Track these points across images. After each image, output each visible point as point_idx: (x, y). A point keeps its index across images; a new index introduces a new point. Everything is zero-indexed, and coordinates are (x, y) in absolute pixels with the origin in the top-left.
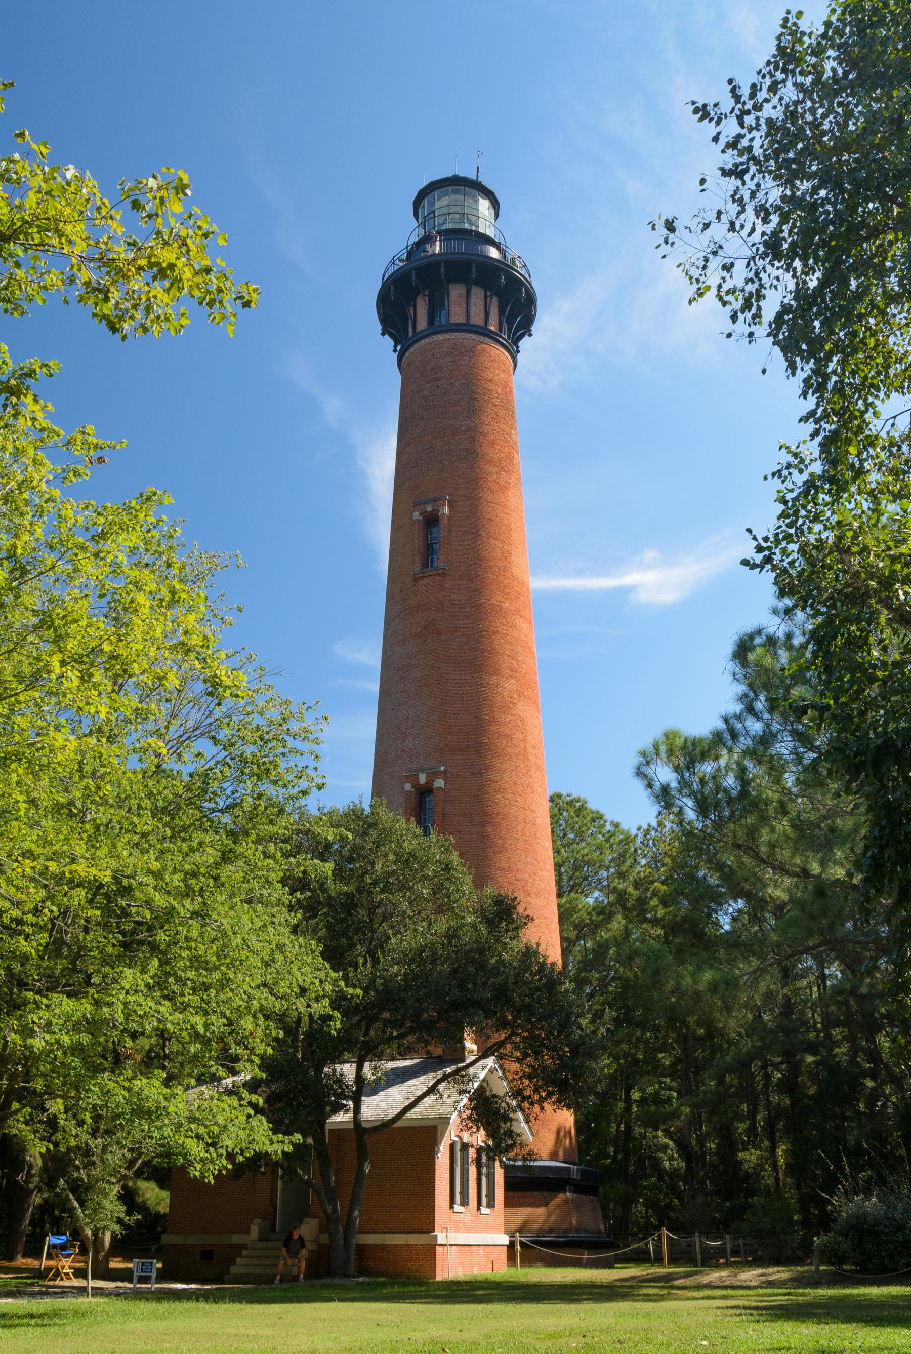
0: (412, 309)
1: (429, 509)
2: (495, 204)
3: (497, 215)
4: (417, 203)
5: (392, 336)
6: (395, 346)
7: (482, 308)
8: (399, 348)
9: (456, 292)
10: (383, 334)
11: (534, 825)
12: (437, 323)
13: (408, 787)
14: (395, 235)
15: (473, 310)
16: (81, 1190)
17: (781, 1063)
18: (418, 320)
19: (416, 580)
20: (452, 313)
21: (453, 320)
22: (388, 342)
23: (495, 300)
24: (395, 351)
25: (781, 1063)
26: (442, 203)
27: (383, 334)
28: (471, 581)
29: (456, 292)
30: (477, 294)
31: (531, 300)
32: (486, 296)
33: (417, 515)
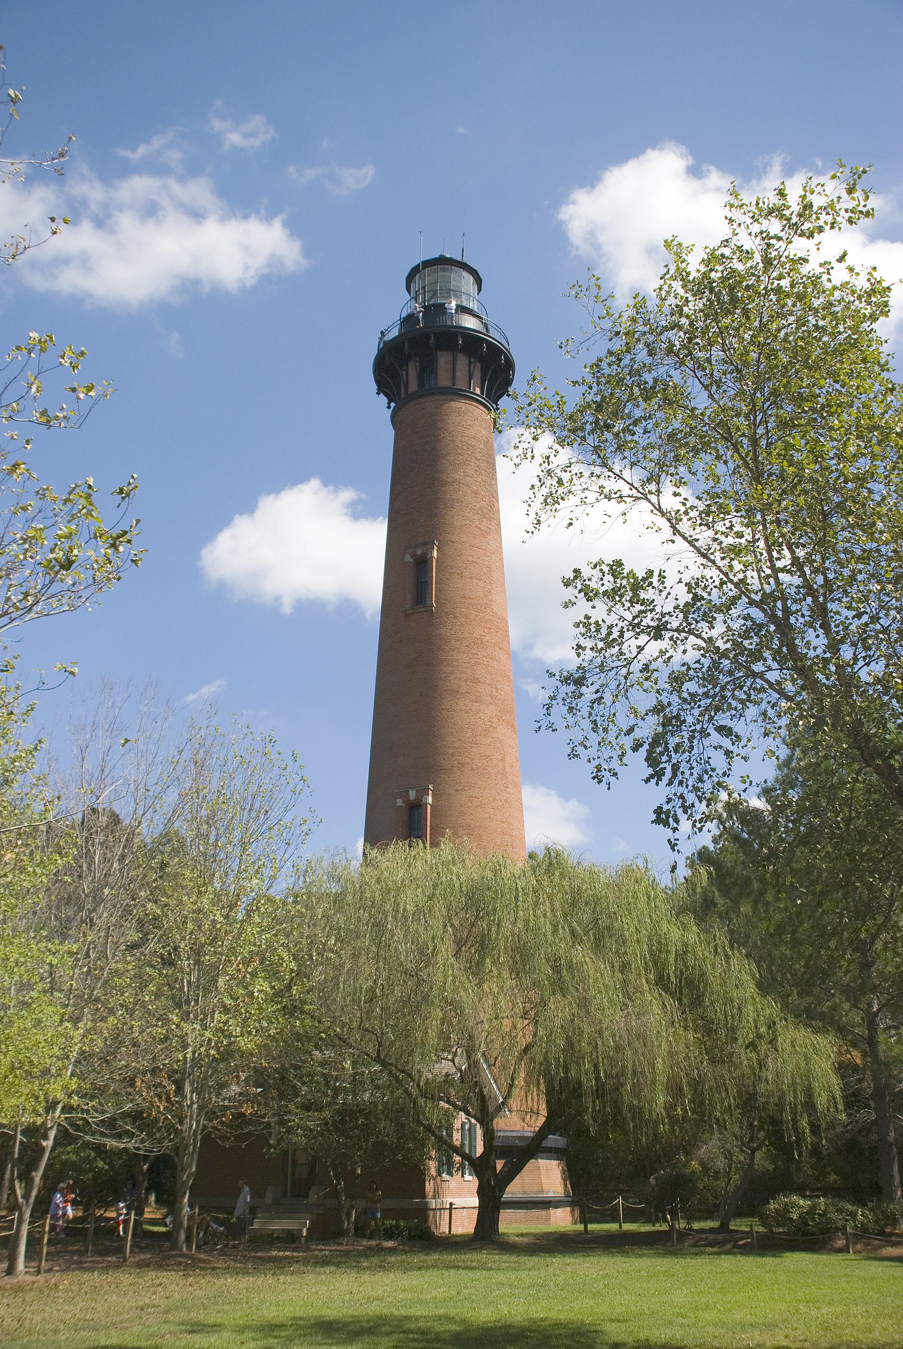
0: (404, 373)
1: (419, 552)
2: (478, 281)
3: (480, 290)
4: (410, 279)
5: (386, 395)
6: (389, 403)
7: (467, 373)
8: (393, 405)
9: (443, 360)
10: (378, 393)
11: (511, 836)
12: (427, 387)
13: (399, 802)
14: (388, 309)
15: (458, 374)
16: (732, 716)
17: (165, 1217)
18: (410, 383)
19: (406, 616)
20: (440, 377)
21: (440, 384)
22: (383, 399)
23: (478, 366)
24: (389, 407)
25: (165, 1217)
26: (428, 276)
27: (378, 393)
28: (456, 617)
29: (443, 360)
30: (462, 361)
31: (510, 365)
32: (470, 363)
33: (408, 558)
